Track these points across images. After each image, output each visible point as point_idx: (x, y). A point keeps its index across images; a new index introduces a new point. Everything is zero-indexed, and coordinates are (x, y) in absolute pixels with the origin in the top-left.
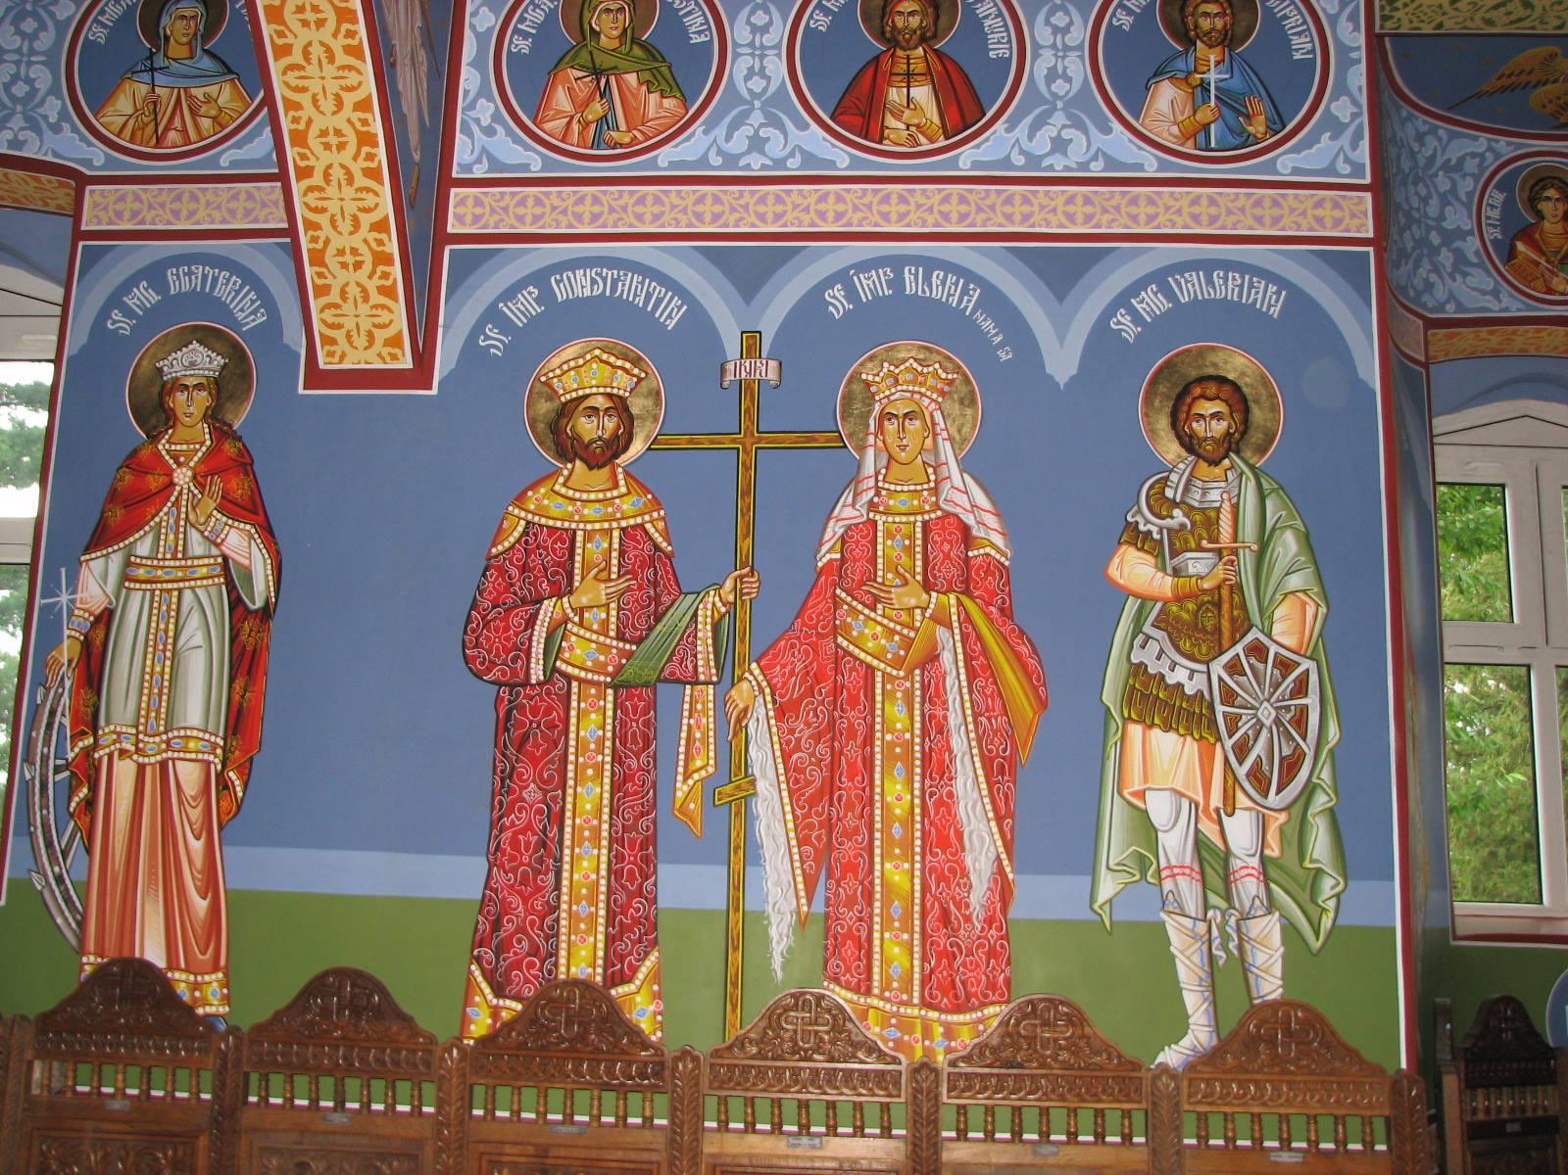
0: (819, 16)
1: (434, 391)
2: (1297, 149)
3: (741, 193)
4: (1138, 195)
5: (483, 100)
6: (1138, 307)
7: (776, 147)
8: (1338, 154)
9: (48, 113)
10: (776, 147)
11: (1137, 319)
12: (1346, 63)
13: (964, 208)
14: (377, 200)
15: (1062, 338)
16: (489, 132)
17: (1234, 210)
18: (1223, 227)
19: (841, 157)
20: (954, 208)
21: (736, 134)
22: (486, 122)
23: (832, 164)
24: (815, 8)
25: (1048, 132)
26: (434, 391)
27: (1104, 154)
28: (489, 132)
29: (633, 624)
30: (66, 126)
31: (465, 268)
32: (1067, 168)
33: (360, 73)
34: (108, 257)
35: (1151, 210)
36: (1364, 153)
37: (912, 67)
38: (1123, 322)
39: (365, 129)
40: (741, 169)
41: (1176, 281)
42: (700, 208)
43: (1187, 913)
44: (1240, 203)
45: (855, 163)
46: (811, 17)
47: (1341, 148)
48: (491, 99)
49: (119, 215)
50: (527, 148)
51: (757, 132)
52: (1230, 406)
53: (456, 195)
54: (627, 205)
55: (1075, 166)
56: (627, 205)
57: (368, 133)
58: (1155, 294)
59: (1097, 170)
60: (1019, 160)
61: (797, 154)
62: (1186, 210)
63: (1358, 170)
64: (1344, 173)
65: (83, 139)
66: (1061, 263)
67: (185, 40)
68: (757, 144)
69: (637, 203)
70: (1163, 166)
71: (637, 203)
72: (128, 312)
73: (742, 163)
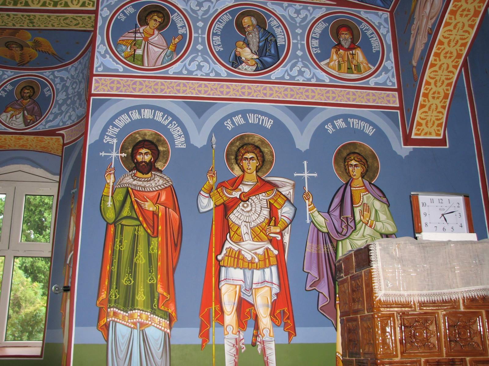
0: (121, 15)
1: (448, 147)
2: (376, 77)
3: (258, 86)
4: (136, 81)
5: (102, 45)
6: (234, 120)
7: (308, 75)
8: (183, 67)
9: (101, 51)
10: (308, 75)
11: (233, 123)
12: (389, 52)
13: (222, 90)
14: (36, 4)
15: (199, 129)
16: (104, 56)
17: (360, 97)
18: (337, 101)
19: (224, 73)
20: (246, 91)
21: (192, 63)
22: (103, 53)
23: (117, 70)
24: (121, 12)
25: (296, 69)
26: (448, 147)
27: (104, 65)
28: (104, 56)
29: (248, 212)
30: (108, 56)
31: (99, 104)
32: (202, 75)
33: (77, 5)
34: (107, 103)
35: (200, 89)
36: (395, 80)
37: (134, 35)
38: (330, 128)
39: (59, 4)
40: (194, 75)
41: (249, 115)
42: (141, 87)
43: (274, 282)
44: (301, 91)
45: (125, 70)
46: (119, 15)
47: (389, 77)
48: (104, 45)
49: (112, 88)
50: (117, 63)
51: (199, 63)
52: (253, 153)
53: (396, 94)
54: (338, 97)
55: (306, 80)
56: (338, 97)
57: (58, 4)
58: (241, 118)
59: (313, 81)
60: (185, 72)
61: (102, 67)
62: (274, 92)
63: (393, 84)
64: (389, 85)
65: (114, 60)
66: (301, 111)
67: (153, 28)
68: (298, 12)
69: (177, 86)
70: (331, 81)
71: (177, 86)
72: (334, 126)
73: (301, 7)
